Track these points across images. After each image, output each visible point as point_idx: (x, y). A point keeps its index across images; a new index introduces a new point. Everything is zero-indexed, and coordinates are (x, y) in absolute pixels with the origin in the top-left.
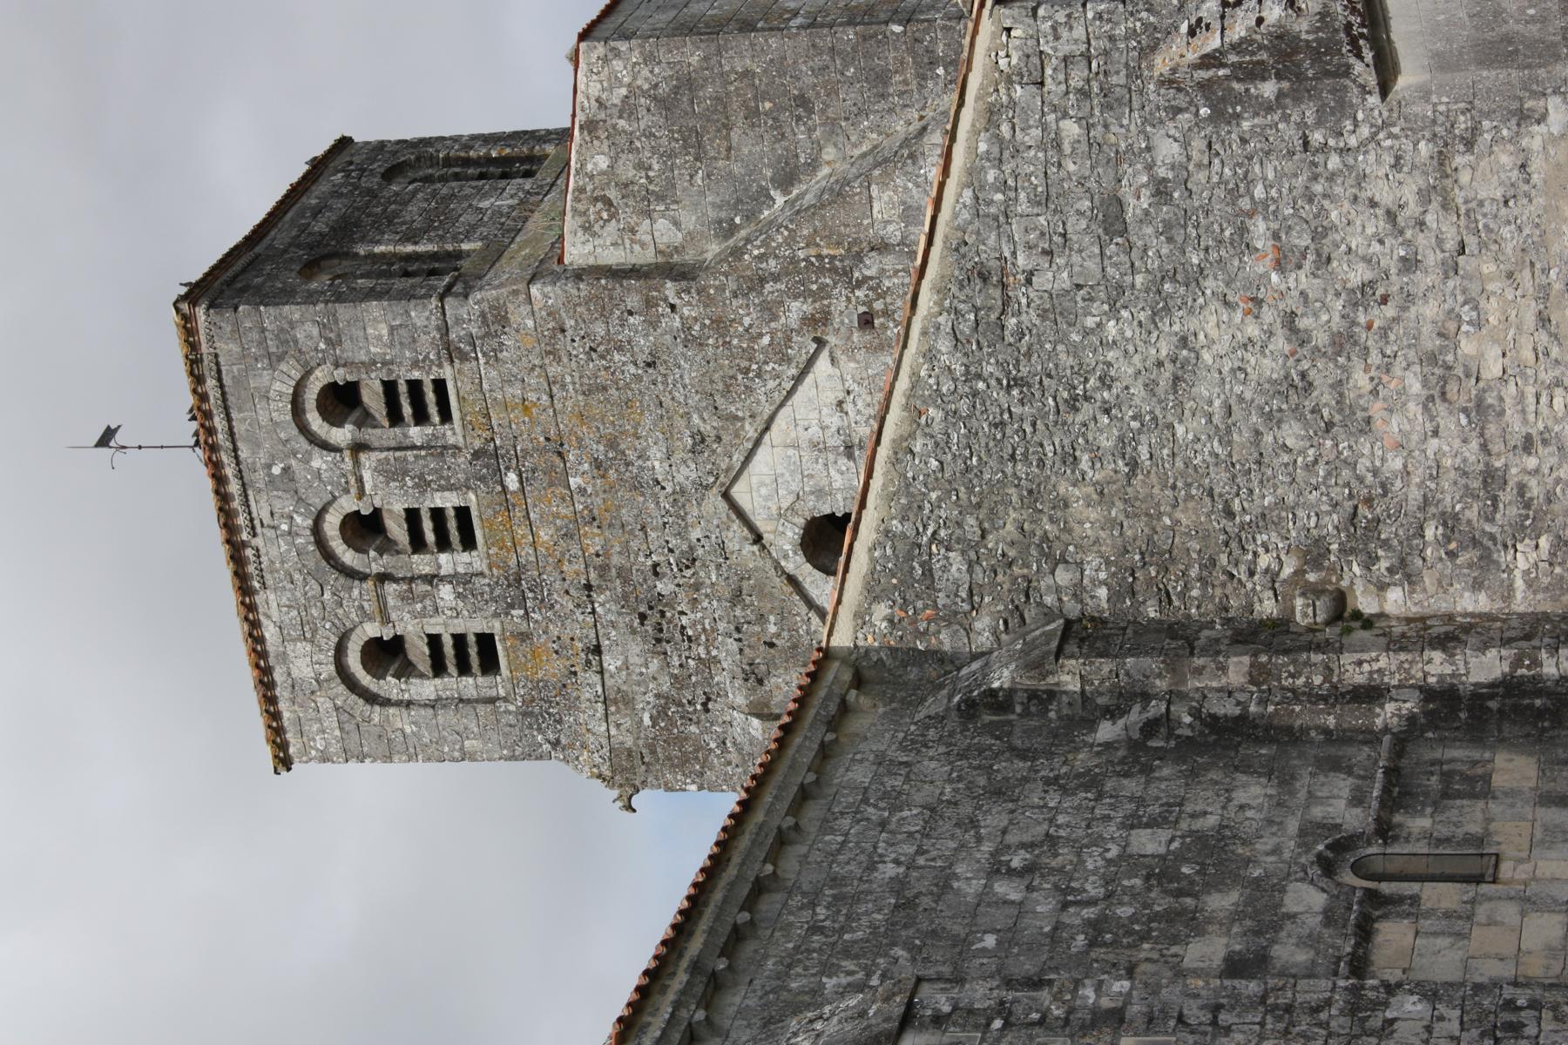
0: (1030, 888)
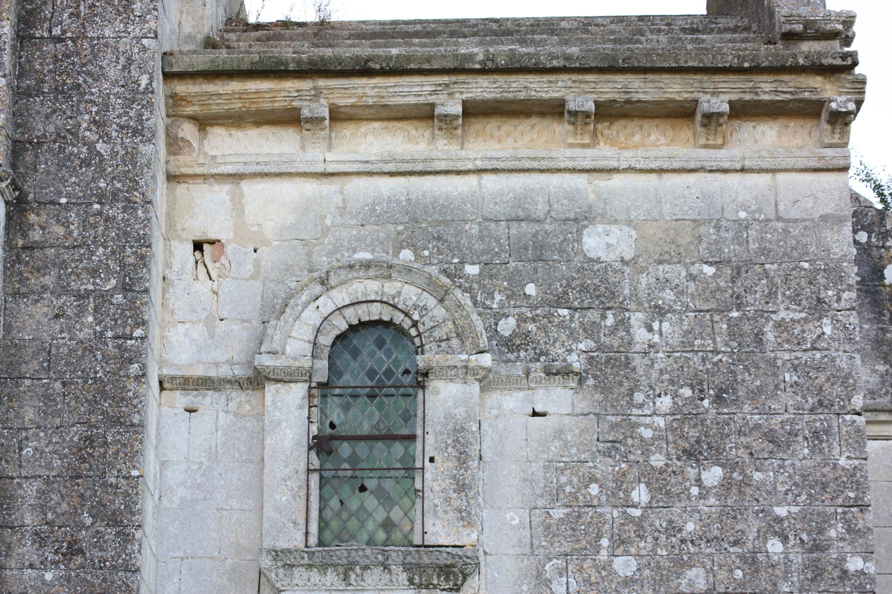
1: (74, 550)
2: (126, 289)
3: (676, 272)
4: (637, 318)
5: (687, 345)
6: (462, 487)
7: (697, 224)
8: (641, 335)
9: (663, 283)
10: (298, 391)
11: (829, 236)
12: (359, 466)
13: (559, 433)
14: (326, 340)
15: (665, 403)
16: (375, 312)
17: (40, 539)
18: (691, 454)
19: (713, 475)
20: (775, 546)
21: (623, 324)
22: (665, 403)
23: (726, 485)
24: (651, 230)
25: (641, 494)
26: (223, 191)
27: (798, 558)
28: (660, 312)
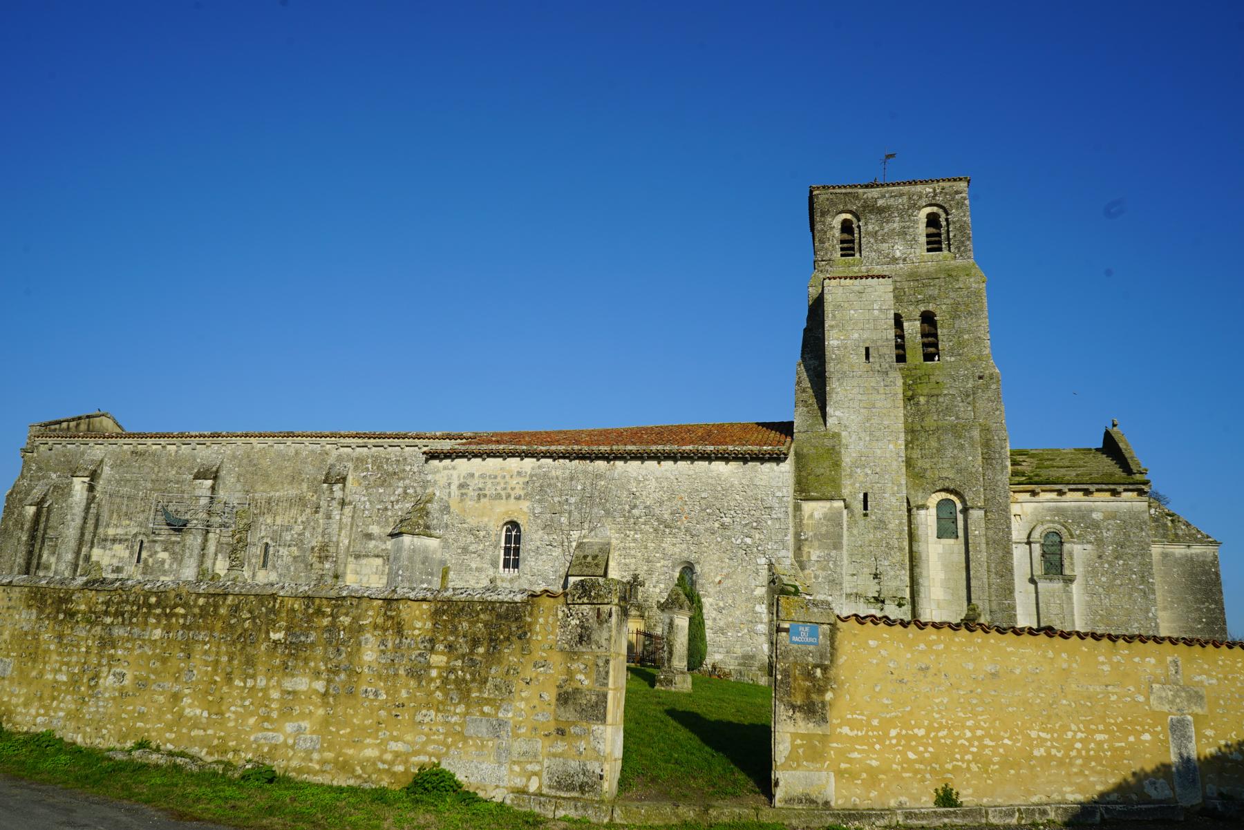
0: (399, 495)
1: (1002, 576)
2: (1008, 528)
3: (1112, 522)
4: (1104, 531)
5: (1114, 536)
6: (1072, 564)
7: (950, 273)
8: (1105, 534)
9: (1109, 524)
10: (1038, 545)
11: (1144, 515)
12: (78, 474)
13: (1089, 553)
14: (1043, 535)
15: (1110, 548)
16: (1052, 530)
17: (996, 574)
18: (1116, 558)
19: (1121, 562)
20: (1134, 576)
21: (1102, 532)
22: (1110, 548)
23: (1124, 564)
24: (1107, 514)
25: (1106, 565)
26: (1019, 505)
27: (1139, 579)
28: (1108, 530)
